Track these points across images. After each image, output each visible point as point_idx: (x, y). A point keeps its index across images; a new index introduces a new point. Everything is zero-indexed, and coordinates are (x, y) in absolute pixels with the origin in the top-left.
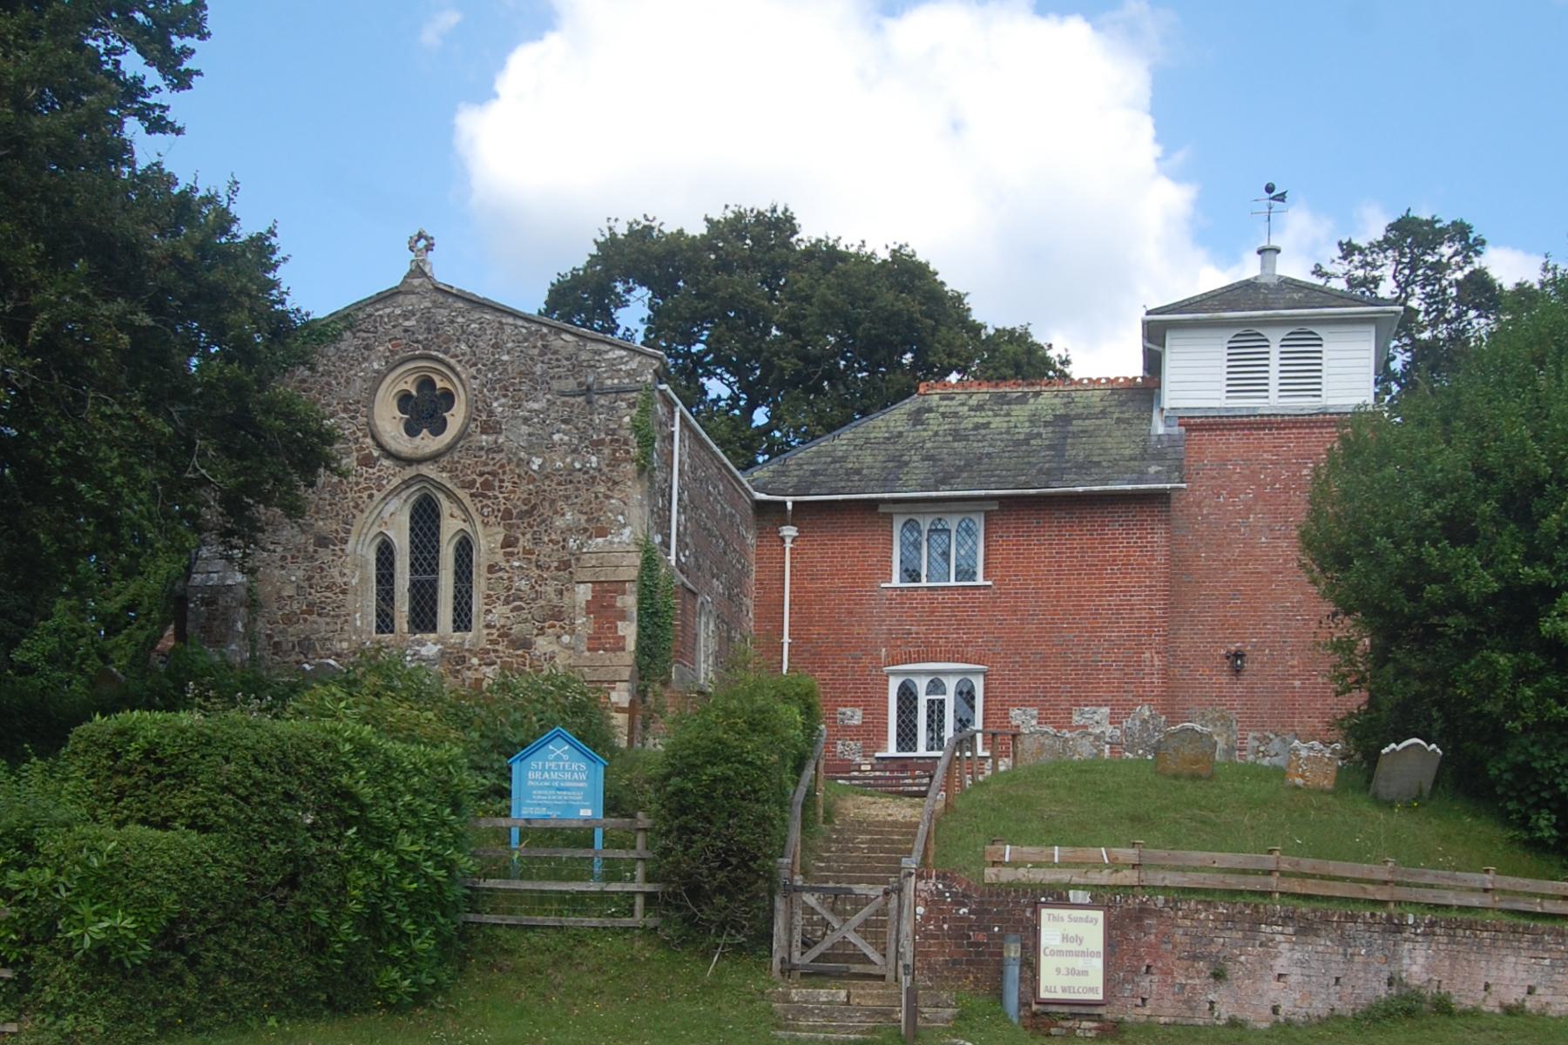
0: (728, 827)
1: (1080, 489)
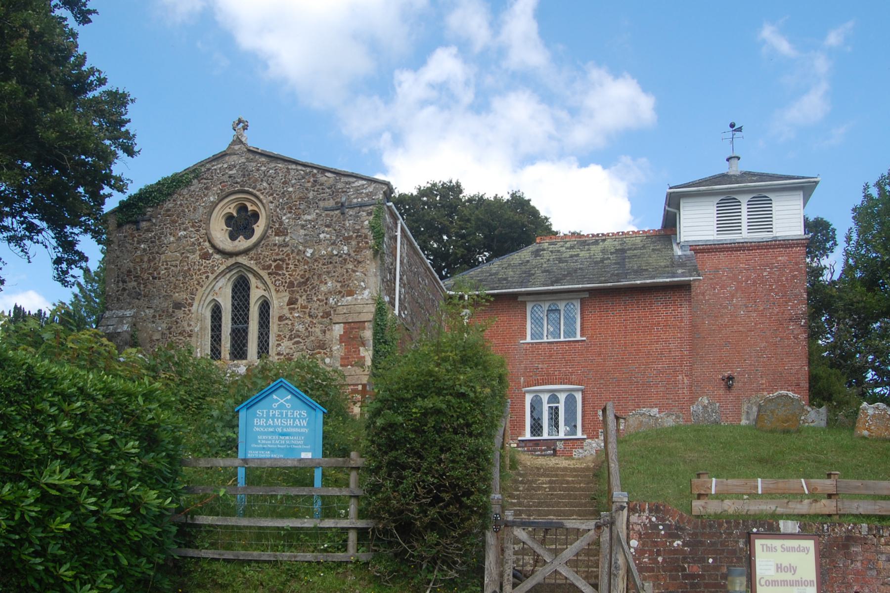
0: (440, 461)
1: (638, 282)
